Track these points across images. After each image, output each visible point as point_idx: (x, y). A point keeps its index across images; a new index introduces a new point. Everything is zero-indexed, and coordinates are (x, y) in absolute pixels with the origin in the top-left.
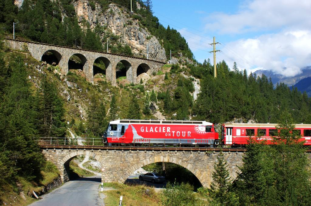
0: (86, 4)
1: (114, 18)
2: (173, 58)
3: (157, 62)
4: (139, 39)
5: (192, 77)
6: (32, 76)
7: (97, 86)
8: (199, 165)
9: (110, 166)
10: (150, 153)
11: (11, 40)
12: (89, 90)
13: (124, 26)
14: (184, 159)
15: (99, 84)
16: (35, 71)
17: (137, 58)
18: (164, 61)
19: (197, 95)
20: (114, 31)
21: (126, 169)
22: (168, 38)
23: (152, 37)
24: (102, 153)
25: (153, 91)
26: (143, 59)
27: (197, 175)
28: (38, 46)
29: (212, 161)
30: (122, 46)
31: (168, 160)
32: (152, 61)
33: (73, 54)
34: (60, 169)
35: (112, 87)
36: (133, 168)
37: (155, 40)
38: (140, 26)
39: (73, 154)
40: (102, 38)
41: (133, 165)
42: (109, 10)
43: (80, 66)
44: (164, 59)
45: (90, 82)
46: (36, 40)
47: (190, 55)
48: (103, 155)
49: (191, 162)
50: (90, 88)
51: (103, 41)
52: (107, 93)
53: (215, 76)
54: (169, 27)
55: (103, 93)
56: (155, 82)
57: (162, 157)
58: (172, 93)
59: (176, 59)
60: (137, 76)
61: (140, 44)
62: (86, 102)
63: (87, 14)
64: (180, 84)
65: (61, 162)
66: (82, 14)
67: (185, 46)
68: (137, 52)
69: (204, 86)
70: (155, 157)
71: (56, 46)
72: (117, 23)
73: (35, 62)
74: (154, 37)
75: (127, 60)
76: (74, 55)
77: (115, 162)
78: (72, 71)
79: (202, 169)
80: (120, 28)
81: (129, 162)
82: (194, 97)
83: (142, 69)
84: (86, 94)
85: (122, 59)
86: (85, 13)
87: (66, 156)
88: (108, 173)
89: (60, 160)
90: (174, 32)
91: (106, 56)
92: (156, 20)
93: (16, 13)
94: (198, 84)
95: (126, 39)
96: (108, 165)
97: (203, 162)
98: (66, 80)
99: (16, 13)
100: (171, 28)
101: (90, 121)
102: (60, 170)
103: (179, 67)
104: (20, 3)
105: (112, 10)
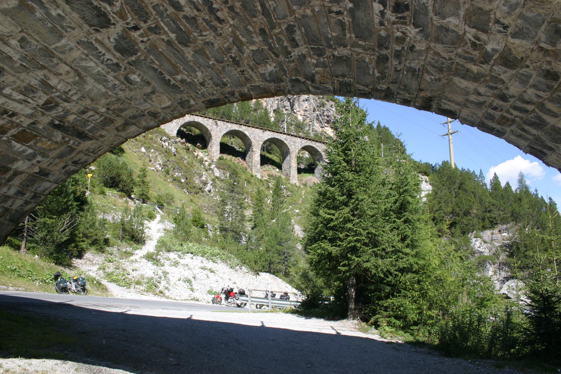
1: (300, 100)
7: (265, 180)
13: (314, 111)
16: (156, 143)
45: (254, 174)
50: (253, 181)
72: (304, 107)
75: (314, 146)
78: (225, 156)
91: (282, 137)
94: (426, 182)
98: (213, 166)
100: (382, 125)
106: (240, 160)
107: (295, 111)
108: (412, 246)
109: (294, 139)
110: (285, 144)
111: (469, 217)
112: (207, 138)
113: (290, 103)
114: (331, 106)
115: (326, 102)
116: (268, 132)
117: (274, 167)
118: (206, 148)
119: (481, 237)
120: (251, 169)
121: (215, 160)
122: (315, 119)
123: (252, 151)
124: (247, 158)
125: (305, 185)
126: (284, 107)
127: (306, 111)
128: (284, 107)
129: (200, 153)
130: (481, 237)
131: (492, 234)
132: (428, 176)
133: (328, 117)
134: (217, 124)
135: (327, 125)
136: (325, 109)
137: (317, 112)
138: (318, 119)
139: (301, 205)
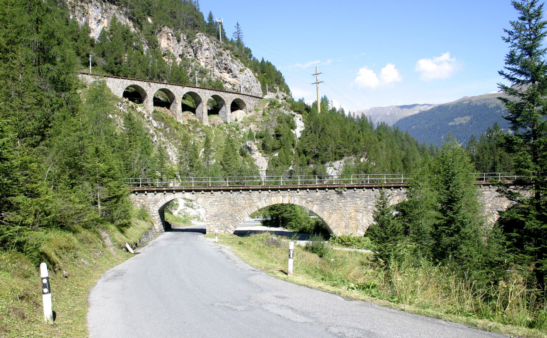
0: (170, 35)
1: (202, 49)
2: (270, 93)
3: (253, 97)
4: (231, 71)
5: (292, 112)
6: (113, 114)
7: (186, 125)
8: (327, 205)
9: (217, 211)
10: (266, 193)
11: (88, 74)
12: (177, 129)
13: (214, 58)
14: (308, 199)
15: (189, 123)
17: (230, 93)
18: (261, 96)
19: (300, 132)
20: (203, 64)
21: (236, 215)
22: (263, 72)
23: (245, 69)
24: (205, 195)
25: (250, 130)
26: (237, 94)
27: (325, 219)
28: (118, 81)
29: (343, 201)
30: (213, 79)
31: (289, 201)
32: (247, 95)
33: (158, 89)
34: (153, 216)
35: (203, 126)
36: (245, 212)
37: (249, 72)
38: (231, 57)
39: (169, 197)
40: (190, 70)
41: (245, 209)
42: (197, 40)
43: (167, 104)
44: (260, 93)
46: (115, 74)
47: (287, 91)
48: (206, 197)
49: (318, 202)
50: (179, 127)
51: (191, 76)
52: (198, 132)
53: (319, 111)
54: (263, 59)
55: (194, 132)
56: (252, 120)
57: (281, 198)
58: (272, 132)
59: (272, 94)
60: (231, 112)
61: (233, 77)
62: (175, 143)
63: (172, 45)
64: (280, 121)
65: (154, 208)
66: (166, 46)
67: (281, 80)
68: (230, 87)
69: (307, 122)
70: (273, 198)
71: (139, 81)
72: (206, 55)
73: (115, 98)
74: (248, 69)
75: (219, 95)
76: (159, 90)
77: (223, 205)
79: (331, 211)
80: (209, 60)
81: (240, 205)
82: (297, 135)
83: (236, 106)
84: (174, 135)
85: (213, 94)
86: (170, 44)
87: (161, 201)
88: (215, 220)
89: (153, 205)
90: (269, 64)
92: (248, 51)
93: (92, 45)
94: (300, 120)
95: (217, 72)
96: (214, 210)
97: (333, 202)
99: (92, 45)
100: (265, 61)
101: (181, 163)
102: (154, 218)
103: (278, 102)
104: (97, 34)
105: (199, 40)
106: (166, 109)
107: (198, 58)
108: (294, 209)
109: (204, 91)
110: (198, 95)
111: (327, 152)
112: (142, 95)
113: (194, 50)
114: (228, 55)
115: (223, 52)
116: (186, 88)
117: (190, 112)
118: (142, 103)
119: (333, 166)
120: (176, 117)
121: (151, 113)
122: (215, 66)
123: (176, 103)
124: (171, 108)
125: (213, 125)
126: (189, 53)
127: (207, 58)
128: (189, 53)
129: (139, 109)
130: (333, 166)
131: (340, 163)
132: (301, 114)
133: (225, 65)
134: (150, 85)
135: (224, 71)
136: (223, 58)
137: (217, 60)
138: (217, 66)
139: (214, 143)
